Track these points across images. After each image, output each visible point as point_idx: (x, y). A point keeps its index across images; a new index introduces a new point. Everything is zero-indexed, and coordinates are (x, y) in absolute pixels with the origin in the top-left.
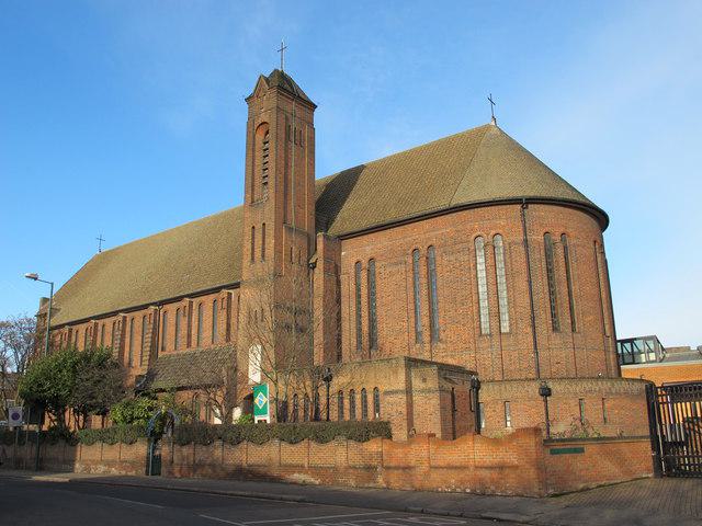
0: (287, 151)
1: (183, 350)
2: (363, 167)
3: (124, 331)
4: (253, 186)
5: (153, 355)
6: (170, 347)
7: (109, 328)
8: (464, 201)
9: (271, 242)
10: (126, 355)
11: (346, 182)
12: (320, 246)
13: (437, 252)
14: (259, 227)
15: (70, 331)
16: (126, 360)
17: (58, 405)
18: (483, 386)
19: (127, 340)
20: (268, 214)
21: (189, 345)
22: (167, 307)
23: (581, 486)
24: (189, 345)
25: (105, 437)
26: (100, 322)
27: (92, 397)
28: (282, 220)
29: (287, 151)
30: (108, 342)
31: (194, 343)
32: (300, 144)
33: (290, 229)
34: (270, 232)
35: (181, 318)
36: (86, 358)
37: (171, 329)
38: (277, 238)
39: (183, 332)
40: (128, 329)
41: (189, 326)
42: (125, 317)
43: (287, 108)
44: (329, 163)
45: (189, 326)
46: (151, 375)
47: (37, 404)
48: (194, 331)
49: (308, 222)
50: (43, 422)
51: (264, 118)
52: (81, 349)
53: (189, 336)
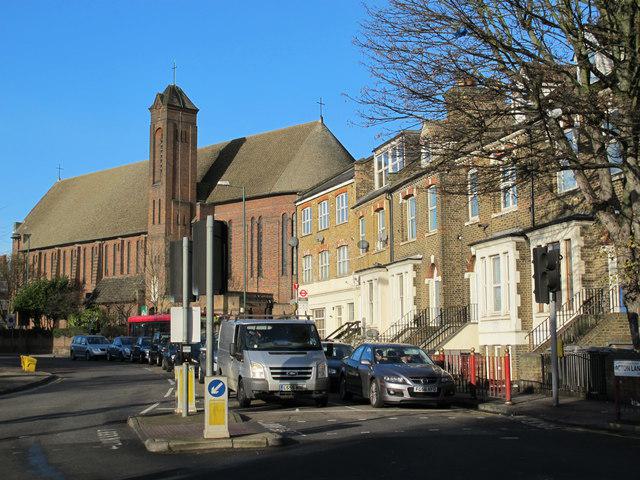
0: (175, 148)
1: (118, 276)
2: (242, 141)
3: (79, 258)
4: (154, 172)
5: (99, 276)
6: (112, 274)
7: (68, 254)
8: (277, 190)
9: (163, 211)
10: (82, 276)
11: (228, 154)
12: (198, 212)
13: (263, 221)
14: (157, 201)
15: (40, 254)
16: (81, 279)
17: (37, 316)
18: (275, 306)
19: (82, 264)
20: (161, 192)
21: (122, 272)
22: (108, 242)
23: (216, 358)
24: (122, 272)
25: (66, 333)
26: (62, 249)
27: (57, 309)
28: (172, 195)
29: (175, 148)
30: (68, 273)
31: (125, 272)
32: (185, 140)
33: (177, 203)
34: (163, 206)
35: (117, 252)
36: (53, 285)
37: (110, 259)
38: (168, 210)
39: (118, 262)
40: (82, 256)
41: (122, 258)
42: (79, 248)
43: (176, 118)
44: (210, 138)
45: (122, 258)
46: (95, 294)
47: (25, 314)
48: (125, 262)
49: (190, 194)
50: (28, 324)
51: (160, 124)
52: (49, 279)
53: (122, 265)
